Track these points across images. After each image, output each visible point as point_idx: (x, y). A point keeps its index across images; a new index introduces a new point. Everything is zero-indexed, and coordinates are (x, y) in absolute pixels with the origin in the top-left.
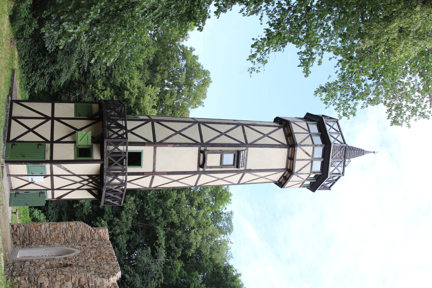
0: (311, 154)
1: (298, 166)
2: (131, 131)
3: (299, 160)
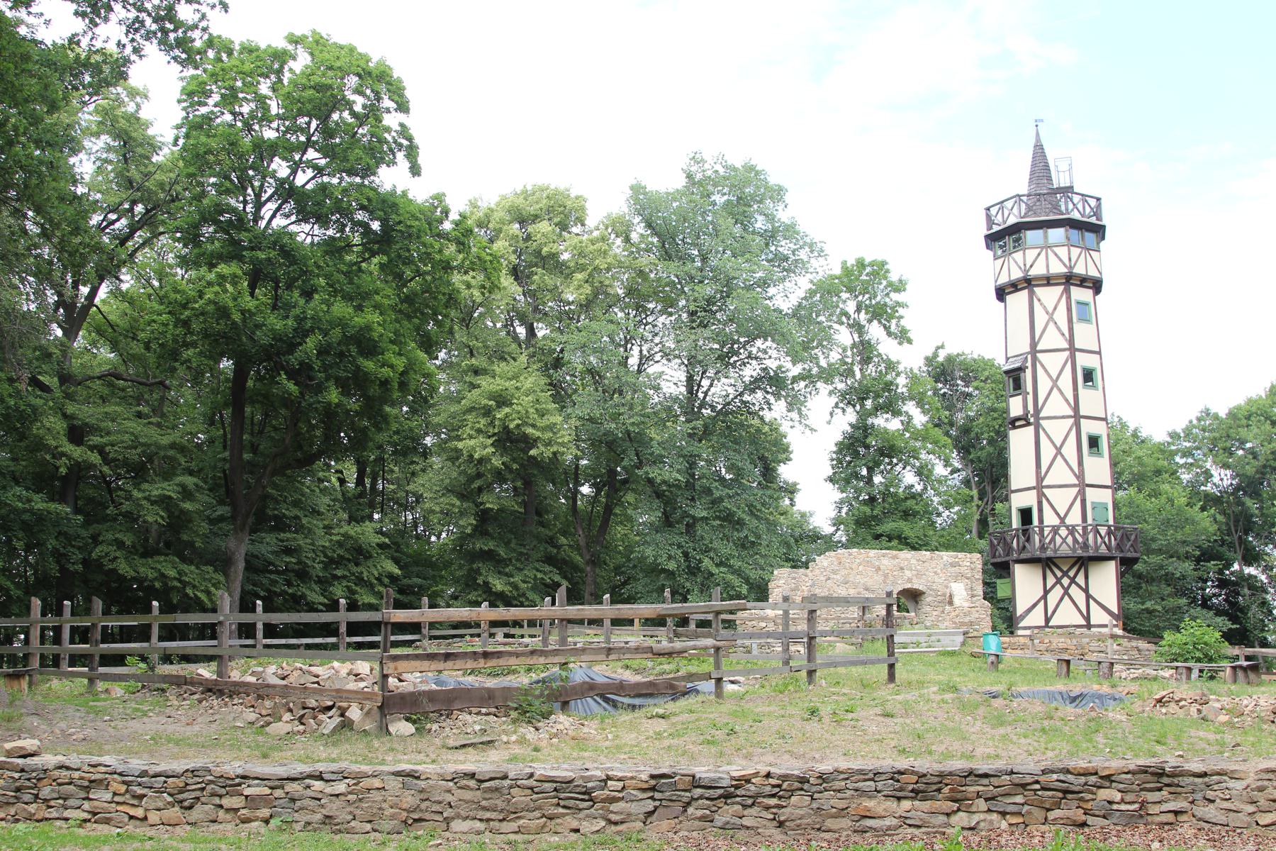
0: (1038, 250)
1: (1057, 268)
2: (1062, 520)
3: (1048, 270)
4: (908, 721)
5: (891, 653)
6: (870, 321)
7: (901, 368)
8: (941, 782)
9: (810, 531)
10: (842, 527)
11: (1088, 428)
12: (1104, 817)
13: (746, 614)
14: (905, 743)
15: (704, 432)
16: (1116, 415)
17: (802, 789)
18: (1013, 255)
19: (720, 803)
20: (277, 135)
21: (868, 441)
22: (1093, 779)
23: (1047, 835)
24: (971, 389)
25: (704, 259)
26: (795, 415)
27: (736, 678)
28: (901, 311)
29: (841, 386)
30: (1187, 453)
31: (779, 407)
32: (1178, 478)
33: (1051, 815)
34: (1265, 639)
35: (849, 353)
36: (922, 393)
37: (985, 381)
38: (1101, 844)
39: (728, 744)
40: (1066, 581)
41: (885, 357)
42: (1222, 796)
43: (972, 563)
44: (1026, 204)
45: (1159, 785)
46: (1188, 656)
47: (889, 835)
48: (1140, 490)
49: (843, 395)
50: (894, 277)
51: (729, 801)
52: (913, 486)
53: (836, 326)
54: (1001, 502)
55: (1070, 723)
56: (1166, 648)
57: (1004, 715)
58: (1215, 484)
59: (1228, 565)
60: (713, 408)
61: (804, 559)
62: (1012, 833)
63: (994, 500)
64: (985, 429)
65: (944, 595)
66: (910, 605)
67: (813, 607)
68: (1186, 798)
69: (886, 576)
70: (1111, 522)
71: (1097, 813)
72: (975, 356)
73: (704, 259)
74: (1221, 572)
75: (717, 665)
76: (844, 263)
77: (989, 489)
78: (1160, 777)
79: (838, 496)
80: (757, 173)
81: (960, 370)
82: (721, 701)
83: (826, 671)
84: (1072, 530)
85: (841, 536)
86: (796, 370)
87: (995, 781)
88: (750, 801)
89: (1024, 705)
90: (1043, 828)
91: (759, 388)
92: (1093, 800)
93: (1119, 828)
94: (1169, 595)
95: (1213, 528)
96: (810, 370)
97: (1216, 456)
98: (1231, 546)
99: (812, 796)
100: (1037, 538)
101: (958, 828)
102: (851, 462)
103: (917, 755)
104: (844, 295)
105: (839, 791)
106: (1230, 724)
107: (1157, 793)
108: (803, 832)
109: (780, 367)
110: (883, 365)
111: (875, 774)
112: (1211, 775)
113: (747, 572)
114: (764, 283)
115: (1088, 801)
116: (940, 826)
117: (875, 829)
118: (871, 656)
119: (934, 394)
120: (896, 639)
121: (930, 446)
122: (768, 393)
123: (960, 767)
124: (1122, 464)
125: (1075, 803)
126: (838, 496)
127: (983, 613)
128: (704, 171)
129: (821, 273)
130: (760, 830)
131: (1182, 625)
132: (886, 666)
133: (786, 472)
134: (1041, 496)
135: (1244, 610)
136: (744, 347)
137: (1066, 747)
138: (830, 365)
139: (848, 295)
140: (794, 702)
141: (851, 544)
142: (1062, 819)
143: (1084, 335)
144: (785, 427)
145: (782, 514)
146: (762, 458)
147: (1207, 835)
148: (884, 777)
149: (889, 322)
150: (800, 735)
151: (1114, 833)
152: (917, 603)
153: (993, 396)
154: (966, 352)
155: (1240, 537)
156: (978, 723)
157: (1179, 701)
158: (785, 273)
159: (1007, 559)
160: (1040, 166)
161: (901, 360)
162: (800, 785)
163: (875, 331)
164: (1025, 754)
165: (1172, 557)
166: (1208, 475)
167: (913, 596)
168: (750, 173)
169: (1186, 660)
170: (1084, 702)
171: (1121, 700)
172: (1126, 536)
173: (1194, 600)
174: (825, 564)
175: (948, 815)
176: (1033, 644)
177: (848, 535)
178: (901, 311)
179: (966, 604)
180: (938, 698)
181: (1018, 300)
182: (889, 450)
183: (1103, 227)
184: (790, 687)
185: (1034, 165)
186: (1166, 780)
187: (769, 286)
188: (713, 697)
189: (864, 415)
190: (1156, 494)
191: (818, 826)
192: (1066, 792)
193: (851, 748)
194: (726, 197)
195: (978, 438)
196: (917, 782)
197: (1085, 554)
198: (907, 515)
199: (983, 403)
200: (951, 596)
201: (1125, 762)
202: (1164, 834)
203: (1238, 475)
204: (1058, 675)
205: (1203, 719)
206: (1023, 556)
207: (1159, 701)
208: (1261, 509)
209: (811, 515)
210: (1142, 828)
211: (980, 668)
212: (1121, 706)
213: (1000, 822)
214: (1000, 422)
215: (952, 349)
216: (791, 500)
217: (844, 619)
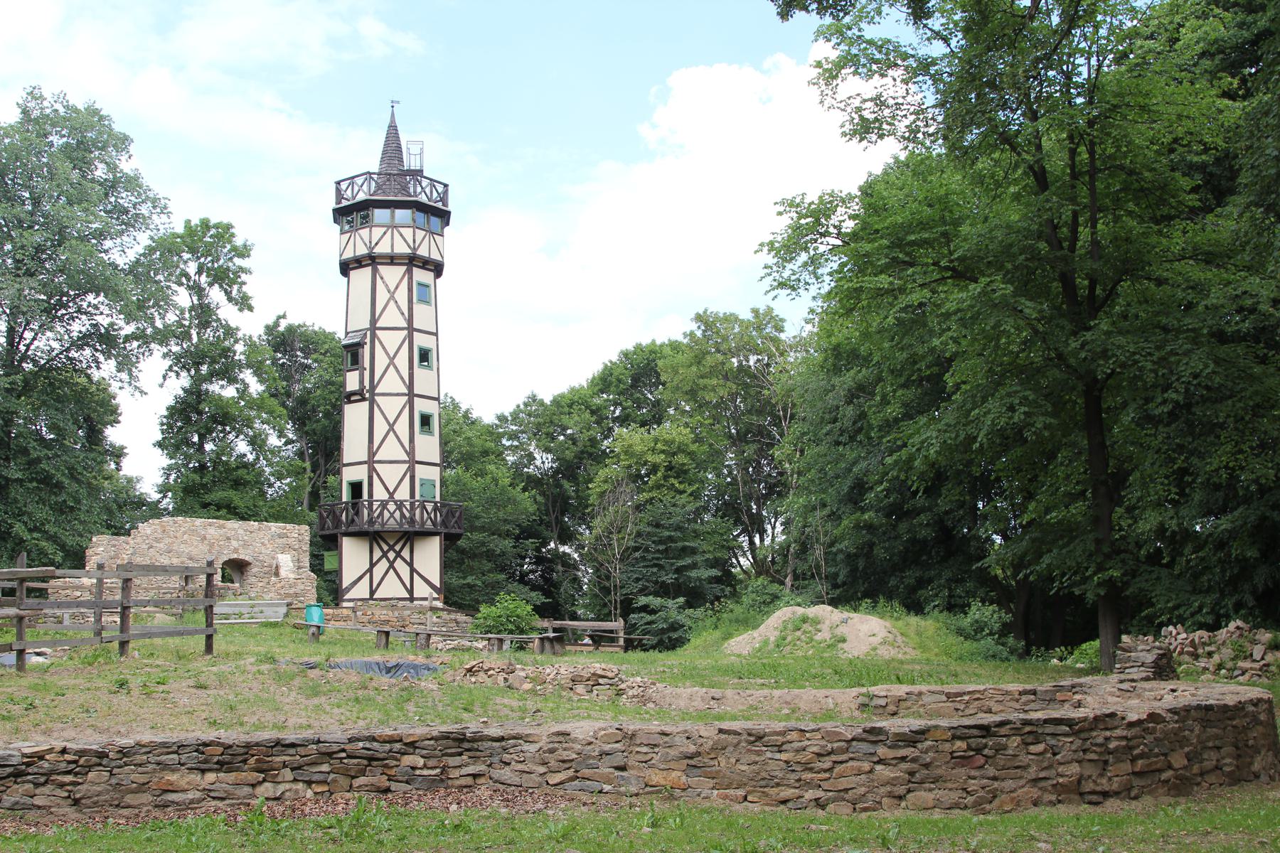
1: (402, 248)
2: (391, 495)
3: (392, 249)
4: (222, 693)
5: (209, 624)
6: (211, 285)
7: (240, 335)
8: (247, 753)
9: (135, 496)
10: (170, 494)
11: (421, 406)
12: (407, 782)
13: (59, 582)
14: (217, 715)
15: (24, 388)
16: (449, 395)
17: (100, 765)
18: (360, 231)
19: (9, 782)
20: (342, 336)
21: (201, 407)
22: (398, 746)
23: (351, 802)
24: (310, 361)
25: (36, 202)
26: (124, 376)
27: (43, 649)
28: (244, 277)
29: (175, 349)
30: (513, 436)
31: (108, 368)
32: (504, 459)
33: (356, 783)
34: (575, 613)
35: (187, 315)
36: (260, 362)
37: (324, 354)
38: (403, 809)
39: (26, 719)
40: (391, 555)
41: (224, 322)
42: (517, 758)
43: (300, 534)
44: (376, 182)
45: (460, 750)
46: (502, 628)
47: (192, 809)
48: (467, 469)
49: (178, 358)
50: (239, 241)
51: (19, 780)
52: (245, 455)
53: (174, 287)
54: (334, 475)
55: (384, 693)
56: (482, 620)
57: (319, 686)
58: (536, 467)
59: (545, 544)
60: (35, 362)
61: (127, 526)
62: (317, 802)
63: (327, 473)
64: (321, 401)
65: (270, 566)
66: (235, 577)
67: (129, 575)
68: (484, 762)
69: (211, 545)
70: (438, 499)
71: (400, 778)
72: (316, 328)
73: (36, 202)
74: (538, 550)
75: (20, 636)
76: (188, 222)
77: (322, 461)
78: (461, 743)
79: (166, 462)
80: (102, 118)
81: (301, 341)
82: (22, 674)
83: (141, 642)
84: (400, 505)
85: (167, 503)
86: (129, 329)
87: (301, 750)
88: (42, 779)
89: (340, 675)
90: (348, 795)
91: (88, 345)
92: (397, 766)
93: (421, 792)
94: (489, 571)
95: (532, 508)
96: (145, 329)
97: (539, 440)
98: (548, 525)
99: (111, 771)
100: (366, 512)
101: (261, 799)
102: (181, 428)
103: (228, 727)
104: (186, 256)
105: (140, 765)
106: (533, 692)
107: (458, 758)
108: (99, 809)
109: (112, 324)
110: (222, 330)
111: (179, 747)
112: (508, 739)
113: (63, 538)
114: (101, 235)
115: (392, 767)
116: (244, 798)
117: (177, 803)
118: (191, 626)
119: (273, 364)
120: (216, 610)
121: (264, 415)
122: (97, 350)
123: (267, 737)
124: (452, 443)
125: (380, 770)
126: (166, 462)
127: (309, 584)
128: (41, 108)
129: (162, 231)
130: (52, 810)
131: (498, 598)
132: (204, 637)
133: (113, 435)
134: (372, 470)
135: (556, 585)
136: (74, 300)
137: (376, 715)
138: (166, 326)
139: (189, 256)
140: (103, 674)
141: (177, 512)
142: (367, 786)
143: (422, 317)
144: (114, 387)
145: (106, 479)
146: (88, 419)
147: (502, 796)
148: (188, 749)
149: (230, 287)
150: (106, 708)
151: (415, 797)
152: (242, 573)
153: (331, 370)
154: (307, 324)
155: (557, 517)
156: (293, 694)
157: (488, 670)
158: (124, 227)
159: (335, 531)
160: (393, 147)
161: (240, 326)
162: (98, 760)
163: (216, 295)
164: (337, 723)
165: (493, 534)
166: (531, 458)
167: (237, 567)
168: (93, 117)
169: (499, 632)
170: (399, 672)
171: (435, 670)
172: (451, 513)
173: (1198, 673)
174: (149, 532)
175: (253, 786)
176: (356, 616)
177: (176, 503)
178: (244, 277)
179: (292, 576)
180: (255, 669)
181: (362, 277)
182: (224, 417)
183: (449, 213)
184: (100, 659)
185: (386, 145)
186: (466, 745)
187: (105, 239)
188: (14, 670)
189: (198, 380)
190: (482, 473)
191: (116, 803)
192: (371, 759)
193: (160, 721)
194: (65, 140)
195: (314, 410)
196: (222, 754)
197: (411, 529)
198: (238, 484)
199: (321, 376)
200: (277, 567)
201: (429, 728)
202: (463, 797)
203: (558, 459)
204: (378, 646)
205: (509, 687)
206: (352, 529)
207: (469, 670)
208: (577, 491)
209: (138, 481)
210: (442, 791)
211: (301, 639)
212: (434, 675)
213: (305, 791)
214: (336, 395)
215: (294, 319)
216: (117, 464)
217: (165, 588)
